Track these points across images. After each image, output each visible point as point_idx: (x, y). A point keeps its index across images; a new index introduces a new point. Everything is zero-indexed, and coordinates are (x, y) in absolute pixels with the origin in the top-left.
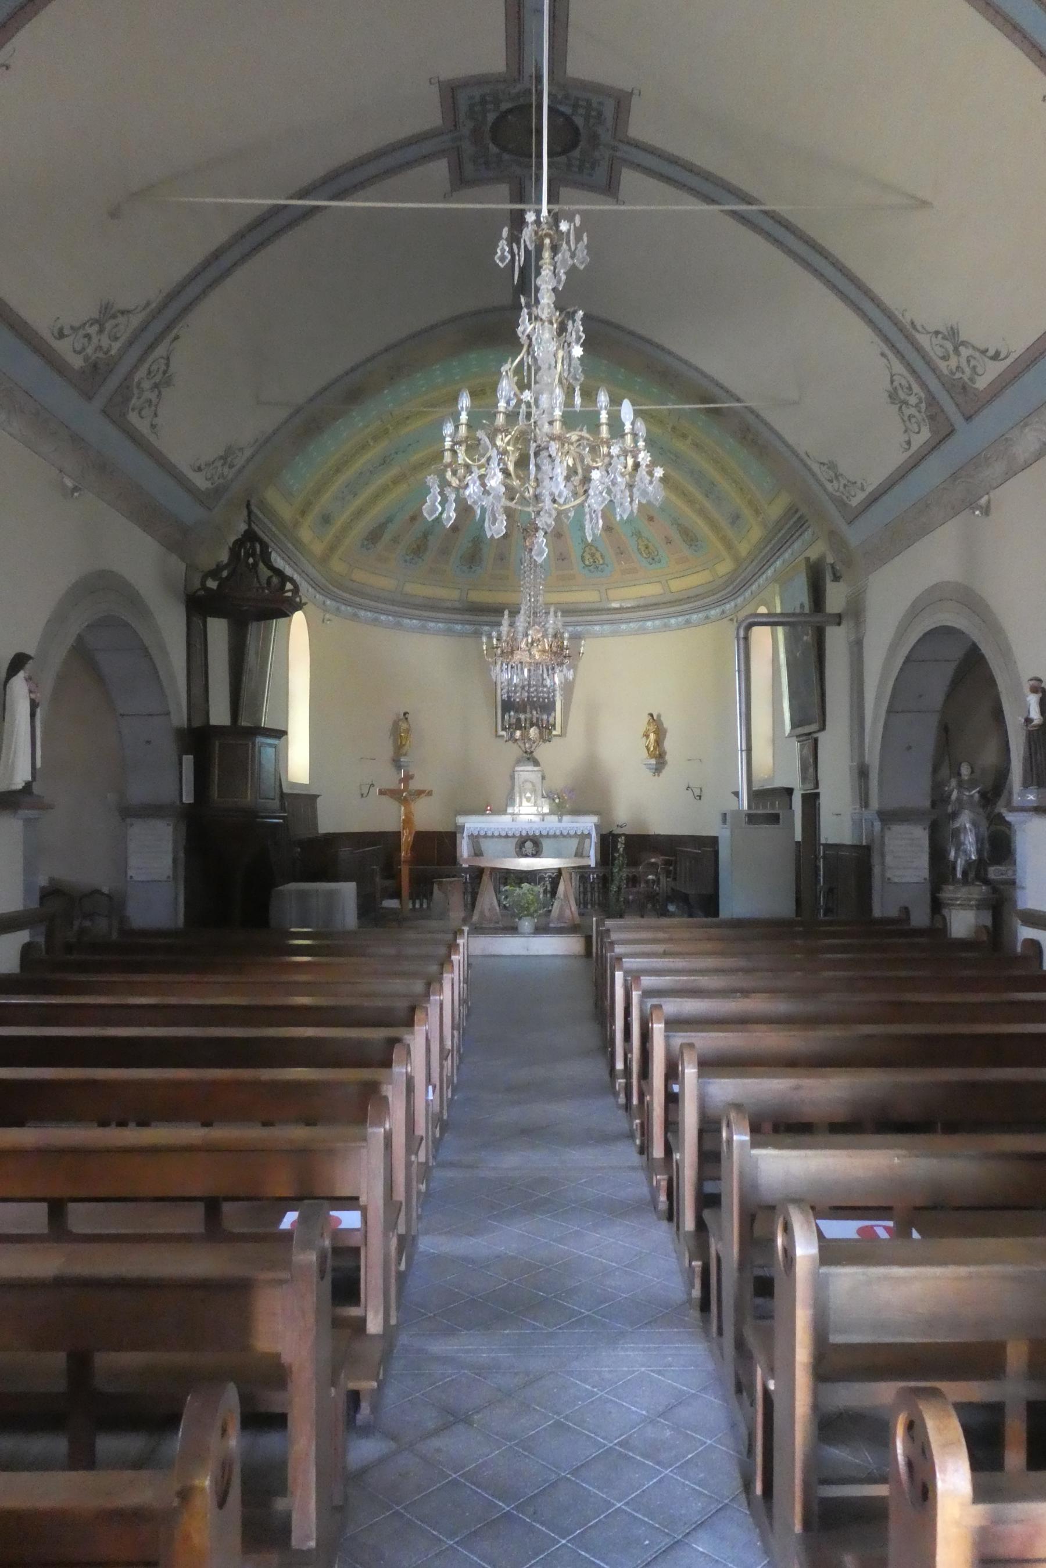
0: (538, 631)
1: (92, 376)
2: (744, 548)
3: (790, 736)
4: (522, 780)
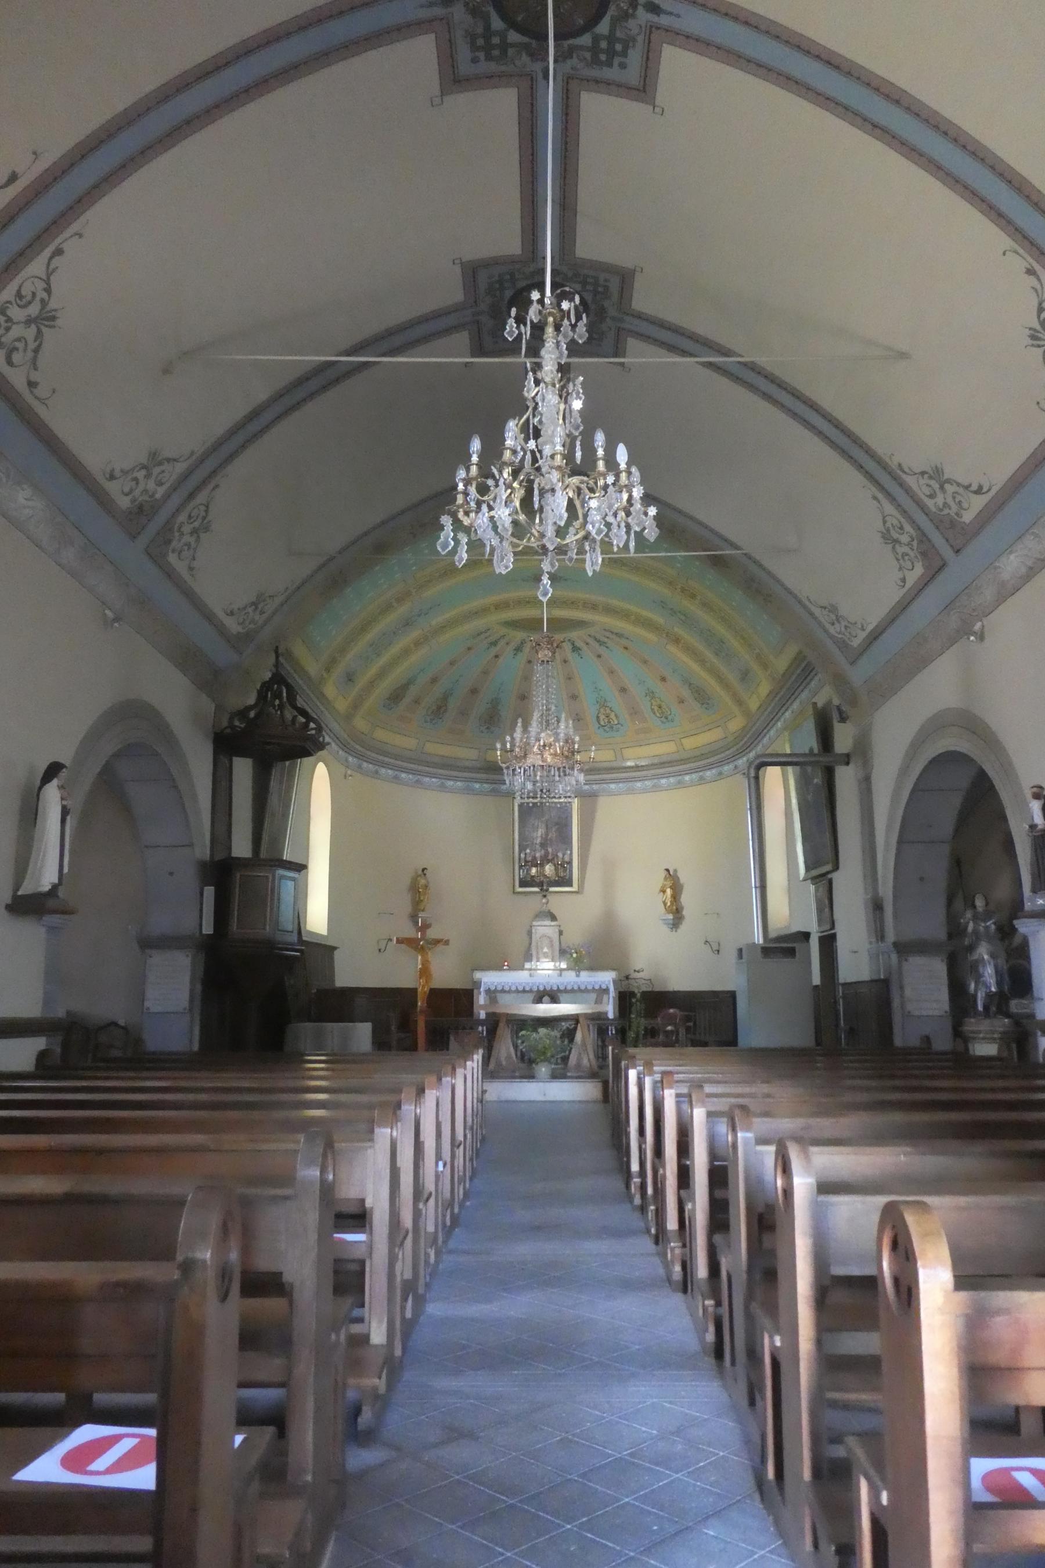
0: (550, 736)
1: (140, 514)
2: (754, 704)
3: (804, 880)
4: (538, 936)
